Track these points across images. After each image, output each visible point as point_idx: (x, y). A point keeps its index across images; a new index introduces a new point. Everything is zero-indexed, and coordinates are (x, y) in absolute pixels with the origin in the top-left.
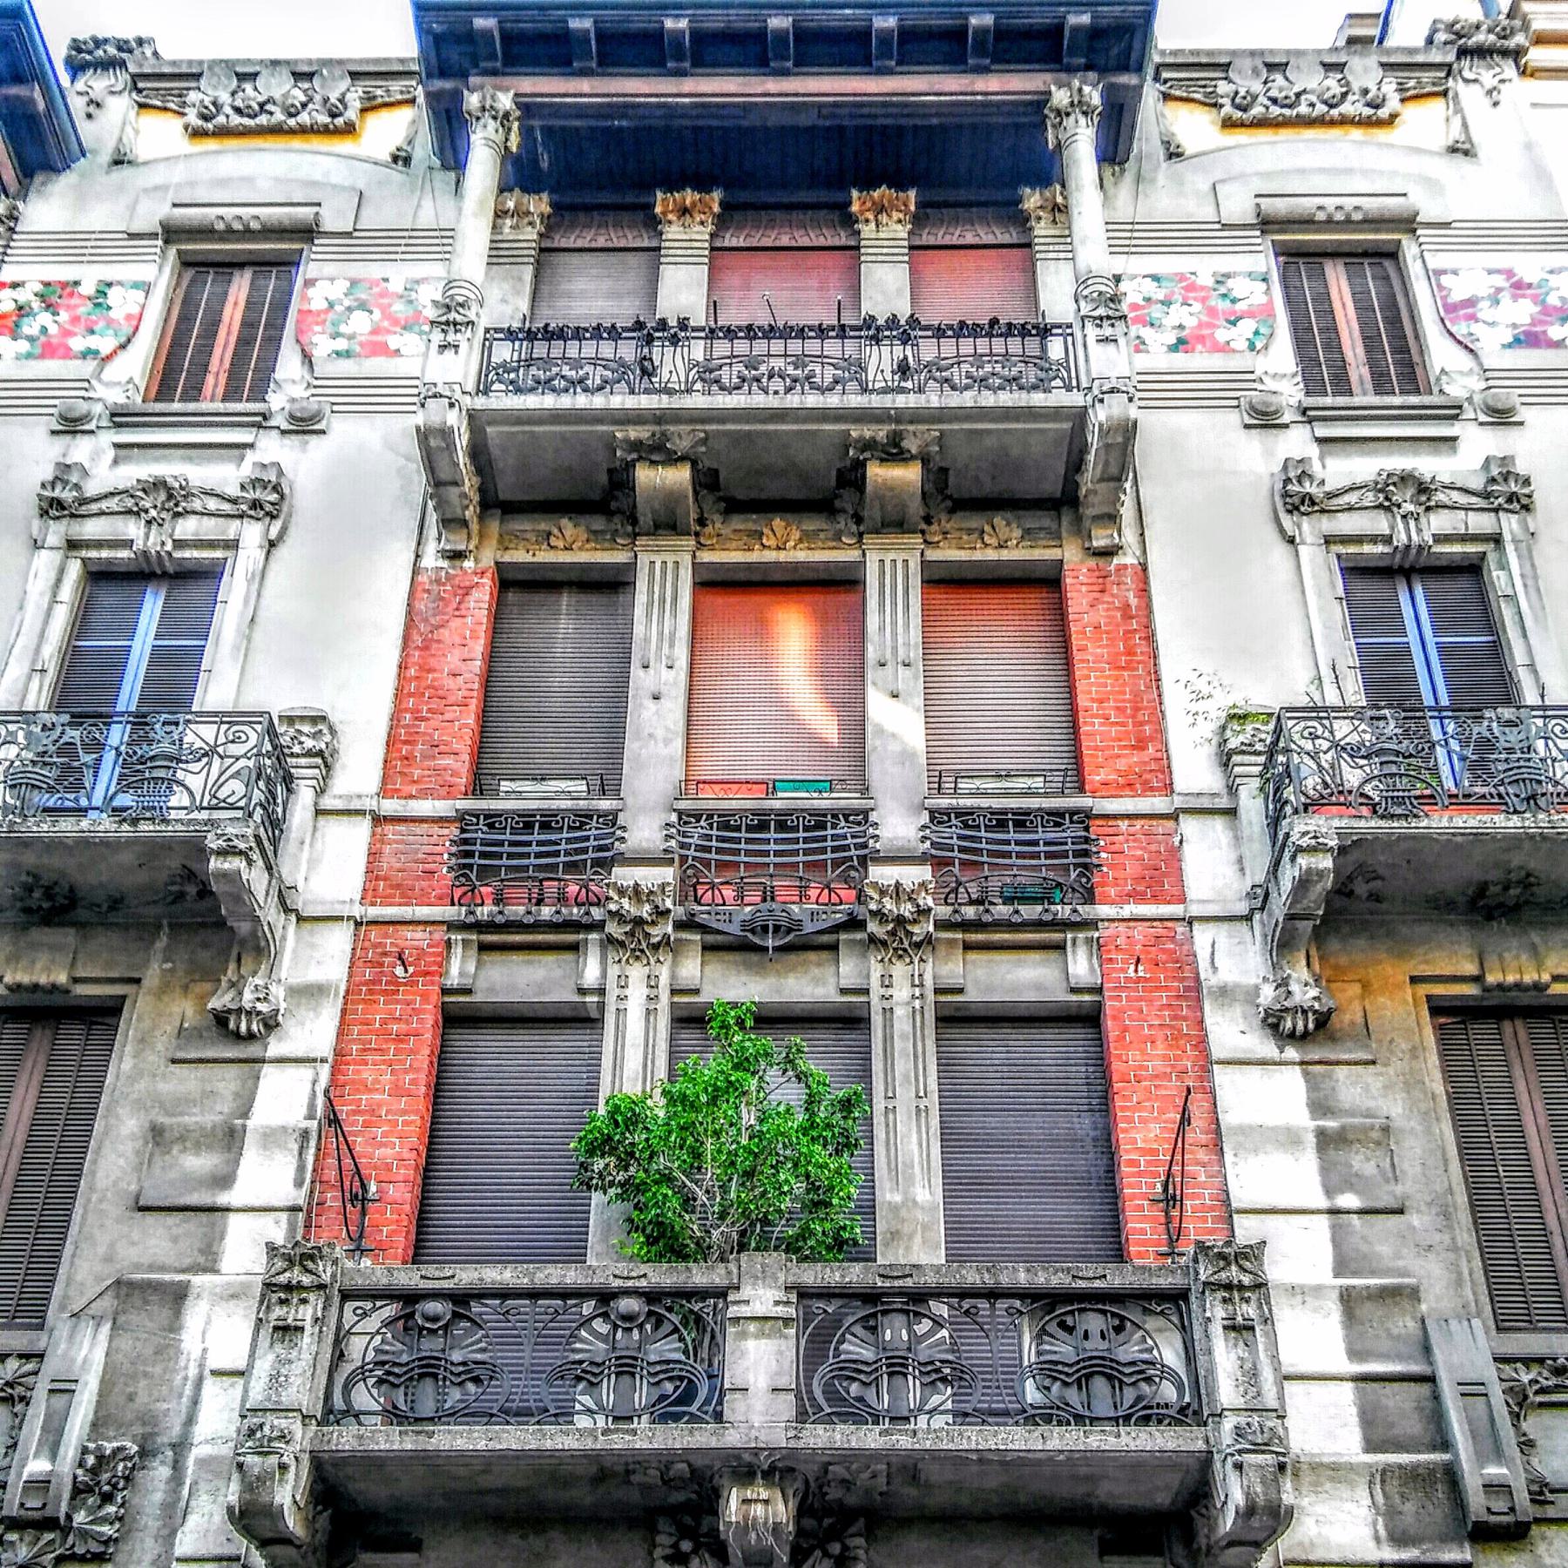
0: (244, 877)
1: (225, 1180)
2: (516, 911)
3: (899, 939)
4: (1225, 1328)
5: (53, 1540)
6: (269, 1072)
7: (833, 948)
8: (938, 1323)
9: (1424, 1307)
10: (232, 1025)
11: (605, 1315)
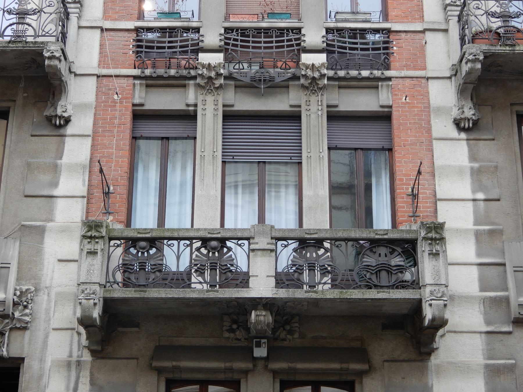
0: (59, 67)
1: (55, 184)
2: (161, 71)
3: (313, 86)
4: (429, 254)
5: (8, 322)
6: (67, 139)
7: (288, 87)
8: (327, 250)
9: (504, 237)
10: (53, 122)
11: (206, 248)
